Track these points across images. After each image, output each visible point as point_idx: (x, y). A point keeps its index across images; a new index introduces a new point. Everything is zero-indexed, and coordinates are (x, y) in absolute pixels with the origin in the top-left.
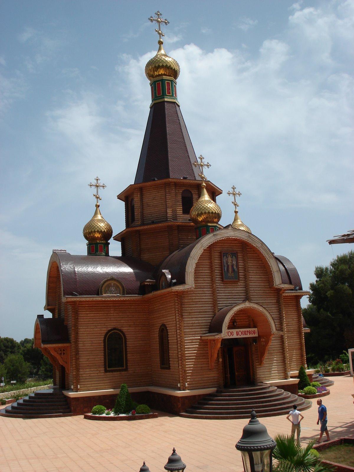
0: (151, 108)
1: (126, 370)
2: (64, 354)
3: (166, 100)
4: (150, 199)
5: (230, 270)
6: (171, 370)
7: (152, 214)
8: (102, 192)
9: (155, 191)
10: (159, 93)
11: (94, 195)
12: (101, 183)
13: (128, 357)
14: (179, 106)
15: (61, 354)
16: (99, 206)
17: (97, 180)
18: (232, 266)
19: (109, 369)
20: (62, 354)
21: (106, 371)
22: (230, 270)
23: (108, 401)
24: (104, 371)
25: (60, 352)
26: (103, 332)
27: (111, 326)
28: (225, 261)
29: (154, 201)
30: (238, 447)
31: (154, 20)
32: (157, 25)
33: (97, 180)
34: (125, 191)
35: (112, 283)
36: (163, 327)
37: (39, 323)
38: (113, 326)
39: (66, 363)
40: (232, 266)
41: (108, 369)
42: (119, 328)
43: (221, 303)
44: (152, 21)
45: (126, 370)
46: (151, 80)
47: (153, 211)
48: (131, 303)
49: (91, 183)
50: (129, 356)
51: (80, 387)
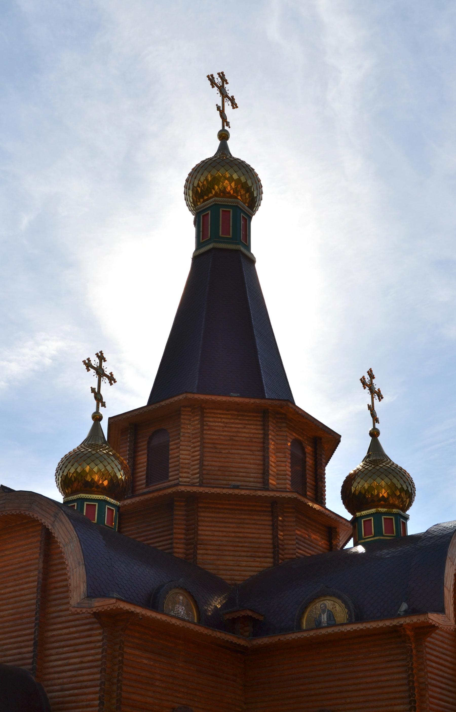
32: (95, 379)
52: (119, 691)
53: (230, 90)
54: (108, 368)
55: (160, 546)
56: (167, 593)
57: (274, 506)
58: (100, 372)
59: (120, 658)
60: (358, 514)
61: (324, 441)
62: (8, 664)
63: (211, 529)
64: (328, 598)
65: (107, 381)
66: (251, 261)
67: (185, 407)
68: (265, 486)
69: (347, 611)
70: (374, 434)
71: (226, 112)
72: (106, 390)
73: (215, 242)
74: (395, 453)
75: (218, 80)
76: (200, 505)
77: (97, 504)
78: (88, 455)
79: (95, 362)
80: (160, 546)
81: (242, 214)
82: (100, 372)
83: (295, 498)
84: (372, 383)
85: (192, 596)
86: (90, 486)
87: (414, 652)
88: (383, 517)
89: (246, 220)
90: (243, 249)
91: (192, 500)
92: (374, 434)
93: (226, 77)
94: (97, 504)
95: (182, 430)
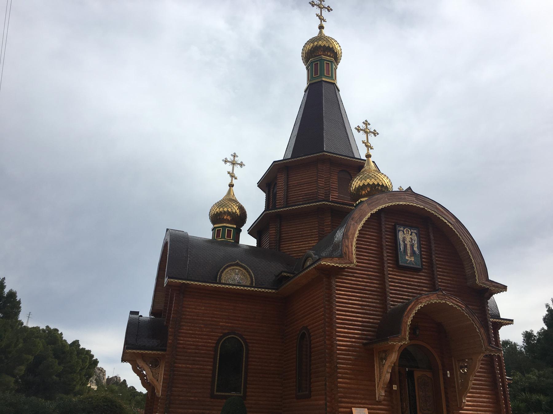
0: (305, 91)
3: (324, 79)
5: (409, 252)
8: (237, 170)
10: (316, 73)
11: (229, 173)
12: (238, 160)
14: (339, 91)
17: (234, 156)
18: (412, 246)
19: (218, 393)
22: (409, 252)
28: (401, 236)
30: (410, 188)
31: (315, 5)
33: (234, 156)
35: (237, 269)
36: (304, 331)
37: (168, 240)
39: (158, 380)
40: (412, 246)
41: (216, 393)
43: (394, 302)
44: (313, 6)
46: (274, 207)
49: (226, 159)
65: (326, 10)
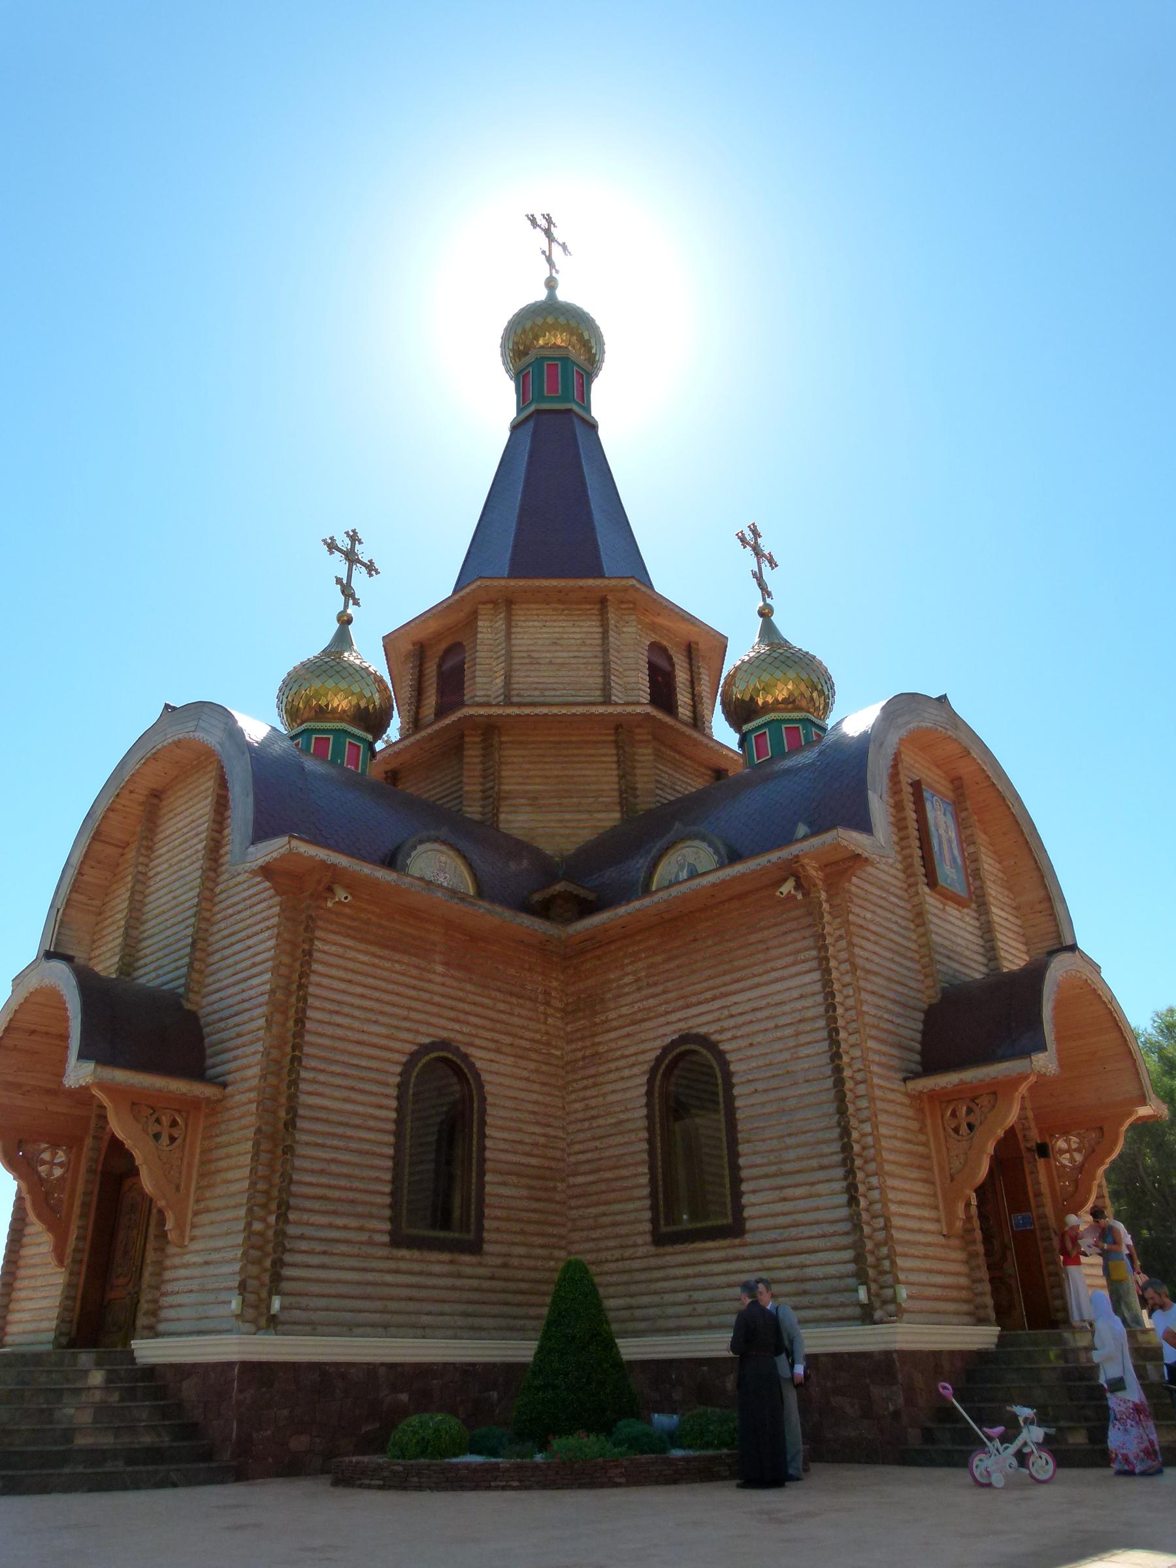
1: (475, 1247)
2: (173, 1139)
4: (540, 642)
6: (748, 1238)
7: (546, 690)
9: (562, 617)
13: (488, 1189)
15: (157, 1136)
16: (349, 621)
20: (165, 1140)
21: (398, 1240)
23: (404, 1397)
24: (386, 1238)
25: (157, 1128)
26: (397, 1045)
27: (431, 1030)
29: (558, 648)
32: (345, 566)
34: (440, 608)
38: (445, 1034)
39: (178, 1188)
42: (463, 1049)
45: (475, 1247)
47: (552, 680)
48: (335, 1049)
50: (495, 1187)
51: (282, 1308)
52: (301, 1004)
53: (765, 544)
54: (364, 552)
55: (448, 802)
56: (414, 848)
57: (622, 731)
58: (351, 557)
59: (306, 947)
60: (745, 728)
61: (703, 645)
62: (164, 988)
63: (520, 772)
64: (689, 843)
66: (593, 427)
67: (485, 603)
68: (607, 702)
69: (716, 858)
70: (765, 613)
71: (554, 258)
72: (360, 577)
73: (538, 402)
74: (796, 632)
75: (543, 223)
76: (503, 739)
77: (331, 737)
78: (323, 668)
79: (344, 542)
80: (448, 802)
81: (575, 368)
82: (351, 557)
83: (648, 714)
84: (756, 542)
85: (464, 857)
86: (322, 713)
87: (825, 906)
88: (783, 726)
89: (582, 376)
90: (575, 408)
91: (490, 729)
92: (765, 613)
93: (554, 220)
94: (331, 737)
95: (479, 636)
